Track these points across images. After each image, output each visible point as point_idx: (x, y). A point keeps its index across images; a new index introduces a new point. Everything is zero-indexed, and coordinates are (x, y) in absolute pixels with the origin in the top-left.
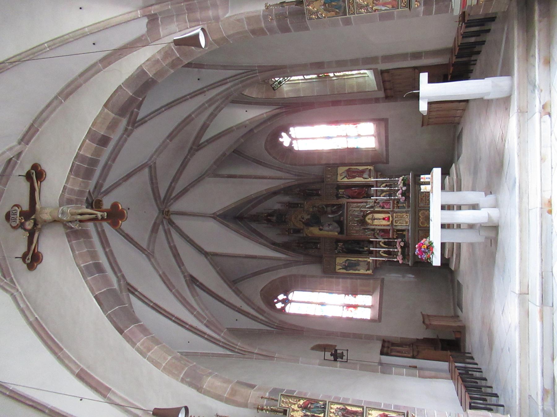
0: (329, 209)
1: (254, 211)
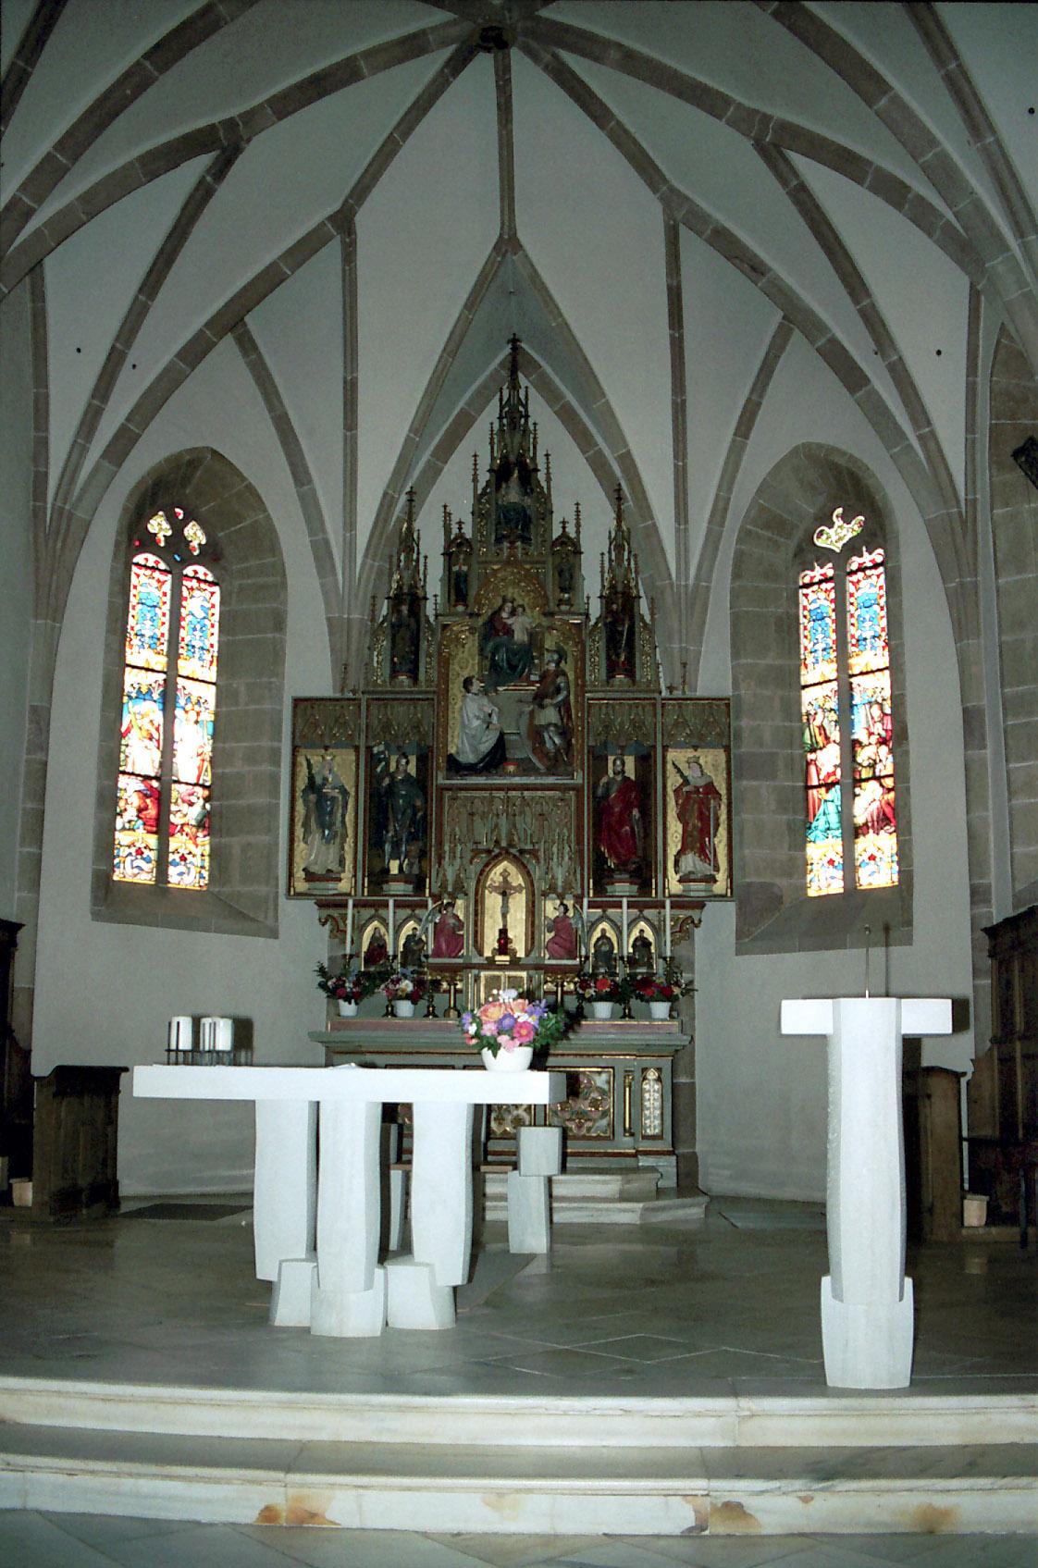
0: (550, 715)
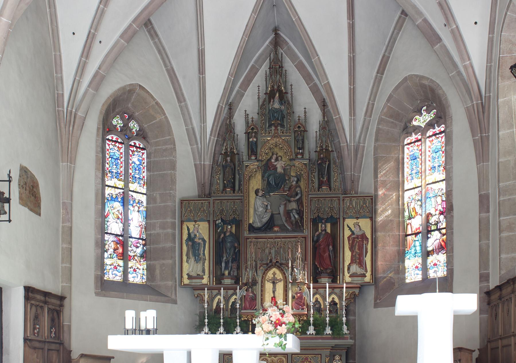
0: (293, 205)
1: (289, 65)
